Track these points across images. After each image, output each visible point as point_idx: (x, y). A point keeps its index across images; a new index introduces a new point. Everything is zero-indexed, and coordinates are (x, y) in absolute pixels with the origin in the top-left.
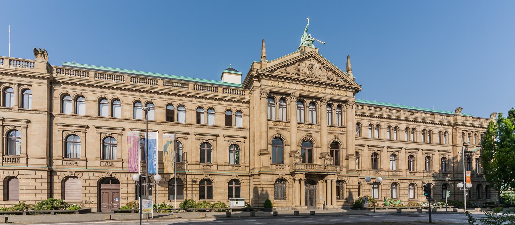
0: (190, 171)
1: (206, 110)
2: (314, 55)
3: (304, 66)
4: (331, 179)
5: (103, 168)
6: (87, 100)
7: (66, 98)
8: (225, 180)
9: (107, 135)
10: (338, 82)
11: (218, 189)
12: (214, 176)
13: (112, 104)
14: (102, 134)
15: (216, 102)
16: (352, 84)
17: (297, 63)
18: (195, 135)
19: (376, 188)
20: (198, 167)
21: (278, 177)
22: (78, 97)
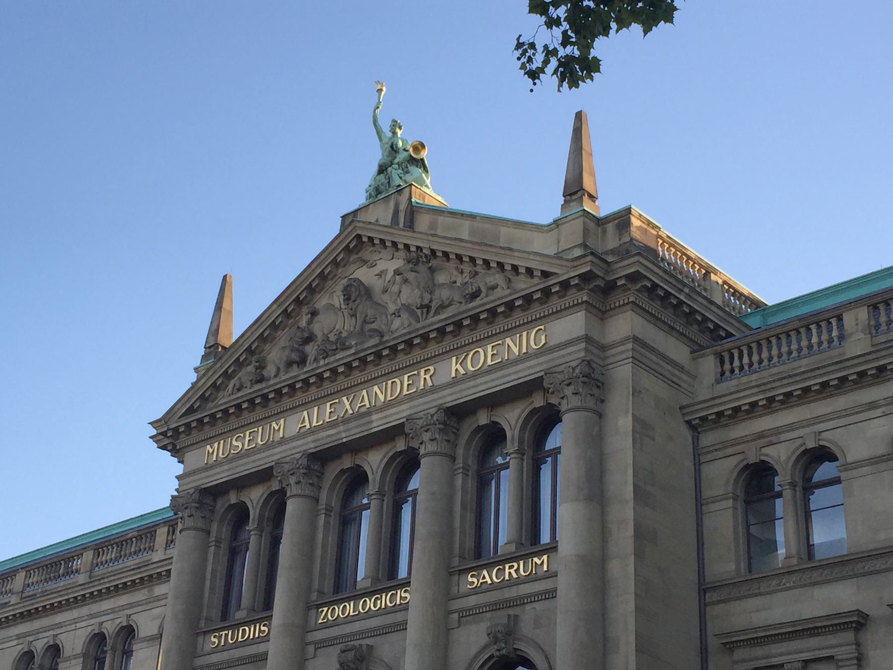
15: (140, 595)
16: (545, 275)
17: (305, 310)
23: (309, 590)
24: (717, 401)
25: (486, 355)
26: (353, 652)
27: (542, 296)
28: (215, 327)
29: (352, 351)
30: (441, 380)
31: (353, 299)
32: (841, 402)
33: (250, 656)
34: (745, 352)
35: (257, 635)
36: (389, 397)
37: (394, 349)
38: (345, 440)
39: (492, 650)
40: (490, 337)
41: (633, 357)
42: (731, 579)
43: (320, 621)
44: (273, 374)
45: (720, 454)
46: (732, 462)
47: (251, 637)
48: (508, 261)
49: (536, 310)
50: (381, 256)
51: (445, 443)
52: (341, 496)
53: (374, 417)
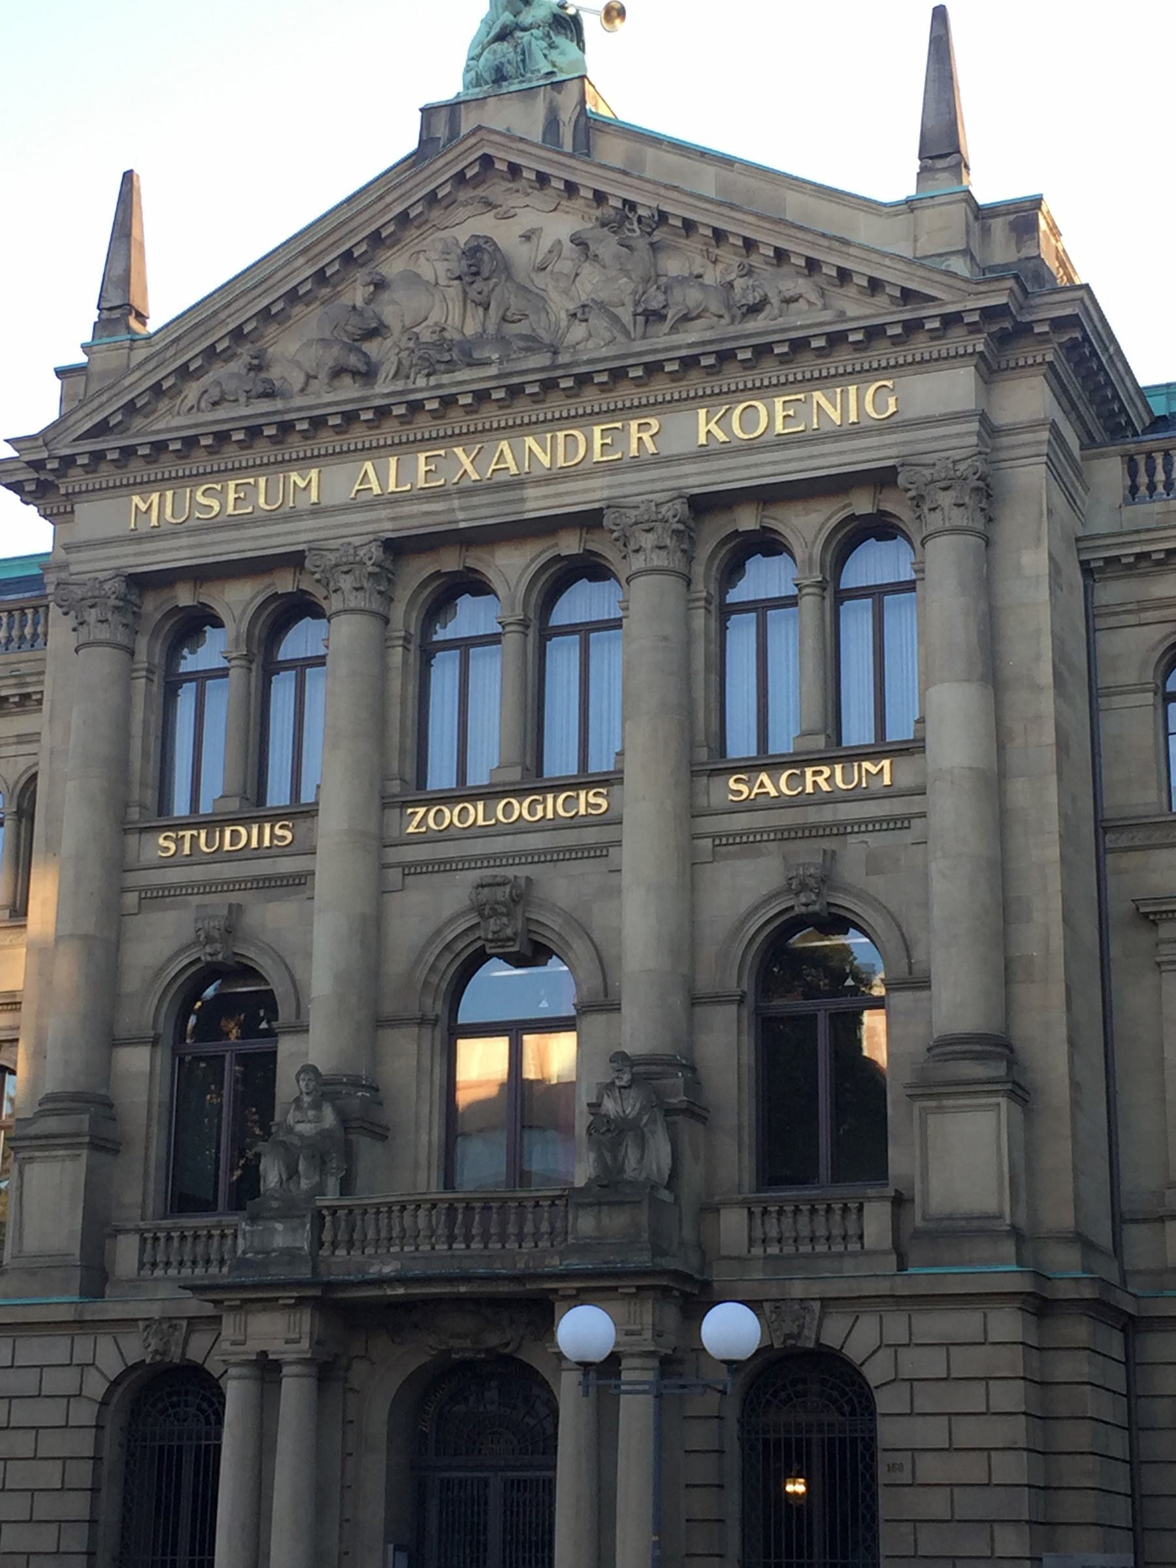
2: (503, 156)
16: (907, 295)
17: (361, 275)
23: (386, 778)
24: (1144, 536)
25: (773, 415)
26: (508, 889)
27: (901, 330)
28: (118, 271)
29: (493, 371)
31: (486, 274)
33: (256, 879)
34: (1159, 462)
35: (267, 843)
36: (552, 458)
37: (583, 380)
38: (462, 525)
40: (780, 387)
41: (1047, 455)
42: (1155, 816)
43: (411, 830)
44: (297, 387)
45: (1131, 619)
46: (1154, 634)
47: (254, 844)
48: (832, 260)
49: (882, 353)
50: (527, 201)
51: (679, 554)
52: (422, 616)
53: (530, 492)
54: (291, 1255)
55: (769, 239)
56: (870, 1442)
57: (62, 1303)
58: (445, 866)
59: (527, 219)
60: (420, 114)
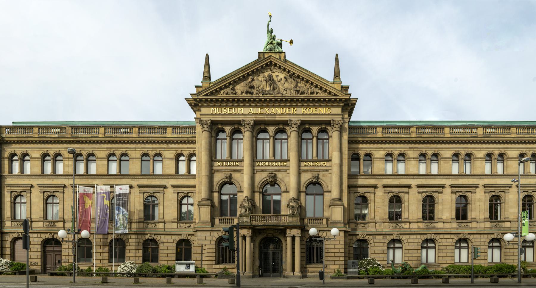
0: (34, 230)
1: (152, 157)
2: (274, 61)
3: (260, 81)
4: (292, 234)
5: (45, 229)
6: (97, 158)
7: (46, 158)
8: (172, 241)
9: (49, 194)
10: (318, 95)
11: (165, 252)
12: (159, 236)
13: (88, 160)
14: (45, 193)
15: (165, 146)
16: (335, 95)
17: (250, 77)
18: (451, 187)
19: (496, 247)
20: (421, 225)
21: (425, 237)
22: (25, 155)
30: (298, 113)
32: (375, 145)
36: (279, 112)
39: (225, 180)
53: (277, 116)
54: (247, 222)
55: (315, 82)
56: (157, 255)
57: (209, 227)
58: (263, 171)
59: (276, 73)
60: (257, 54)
